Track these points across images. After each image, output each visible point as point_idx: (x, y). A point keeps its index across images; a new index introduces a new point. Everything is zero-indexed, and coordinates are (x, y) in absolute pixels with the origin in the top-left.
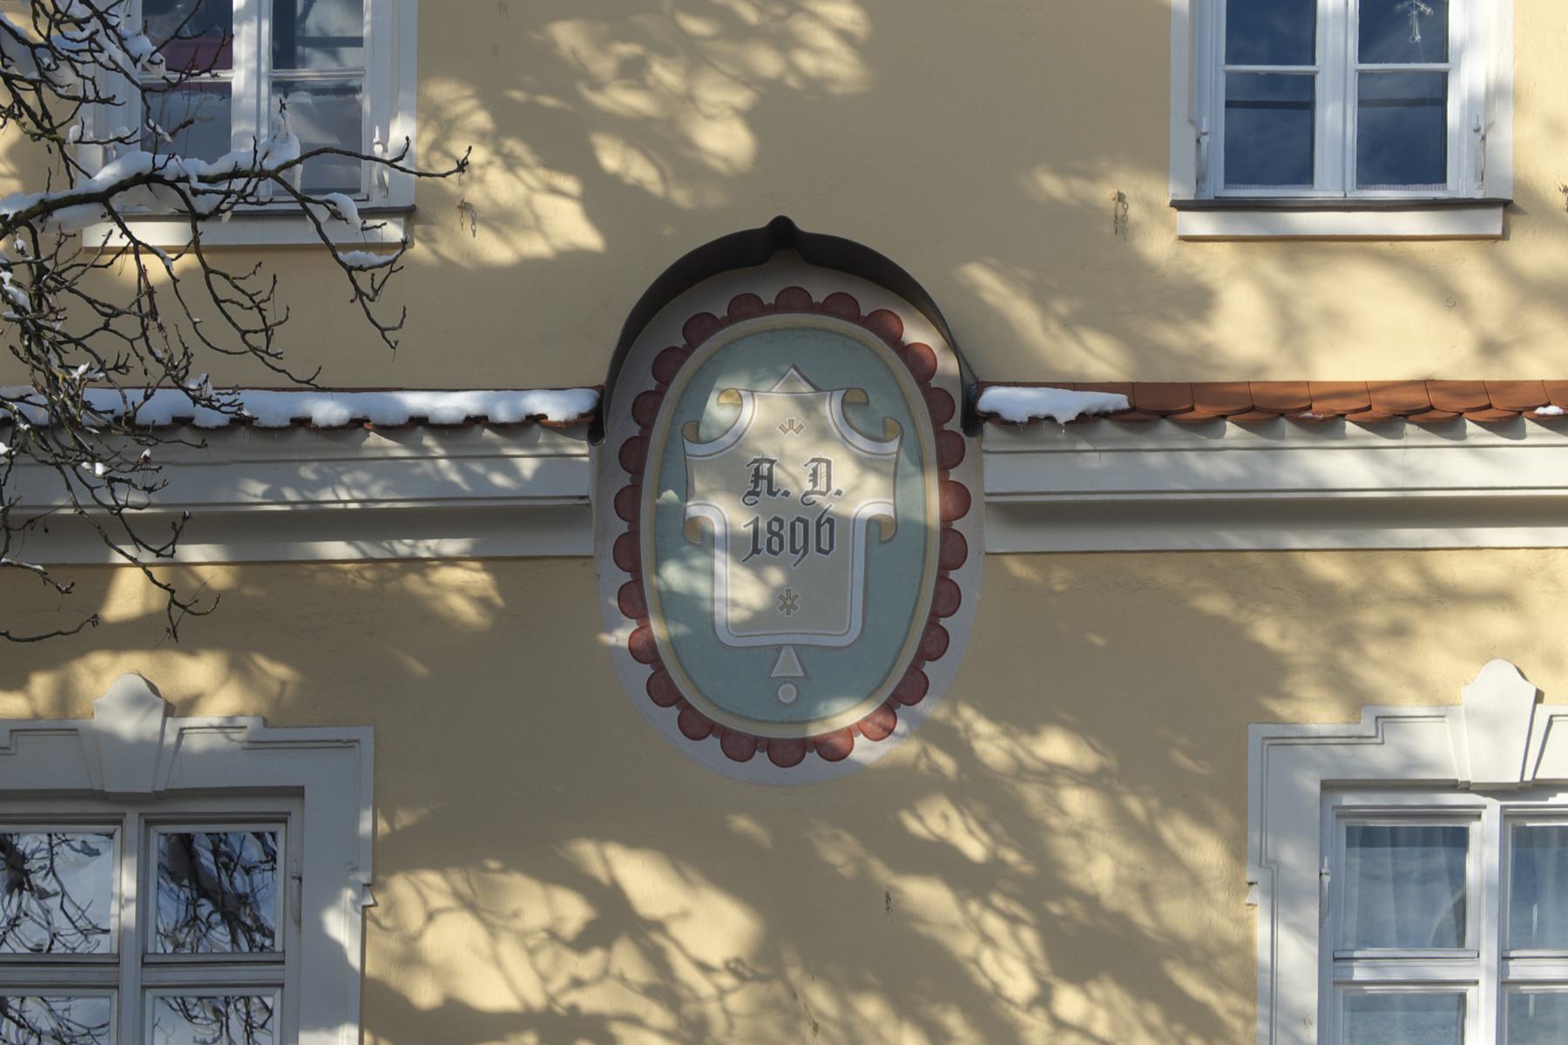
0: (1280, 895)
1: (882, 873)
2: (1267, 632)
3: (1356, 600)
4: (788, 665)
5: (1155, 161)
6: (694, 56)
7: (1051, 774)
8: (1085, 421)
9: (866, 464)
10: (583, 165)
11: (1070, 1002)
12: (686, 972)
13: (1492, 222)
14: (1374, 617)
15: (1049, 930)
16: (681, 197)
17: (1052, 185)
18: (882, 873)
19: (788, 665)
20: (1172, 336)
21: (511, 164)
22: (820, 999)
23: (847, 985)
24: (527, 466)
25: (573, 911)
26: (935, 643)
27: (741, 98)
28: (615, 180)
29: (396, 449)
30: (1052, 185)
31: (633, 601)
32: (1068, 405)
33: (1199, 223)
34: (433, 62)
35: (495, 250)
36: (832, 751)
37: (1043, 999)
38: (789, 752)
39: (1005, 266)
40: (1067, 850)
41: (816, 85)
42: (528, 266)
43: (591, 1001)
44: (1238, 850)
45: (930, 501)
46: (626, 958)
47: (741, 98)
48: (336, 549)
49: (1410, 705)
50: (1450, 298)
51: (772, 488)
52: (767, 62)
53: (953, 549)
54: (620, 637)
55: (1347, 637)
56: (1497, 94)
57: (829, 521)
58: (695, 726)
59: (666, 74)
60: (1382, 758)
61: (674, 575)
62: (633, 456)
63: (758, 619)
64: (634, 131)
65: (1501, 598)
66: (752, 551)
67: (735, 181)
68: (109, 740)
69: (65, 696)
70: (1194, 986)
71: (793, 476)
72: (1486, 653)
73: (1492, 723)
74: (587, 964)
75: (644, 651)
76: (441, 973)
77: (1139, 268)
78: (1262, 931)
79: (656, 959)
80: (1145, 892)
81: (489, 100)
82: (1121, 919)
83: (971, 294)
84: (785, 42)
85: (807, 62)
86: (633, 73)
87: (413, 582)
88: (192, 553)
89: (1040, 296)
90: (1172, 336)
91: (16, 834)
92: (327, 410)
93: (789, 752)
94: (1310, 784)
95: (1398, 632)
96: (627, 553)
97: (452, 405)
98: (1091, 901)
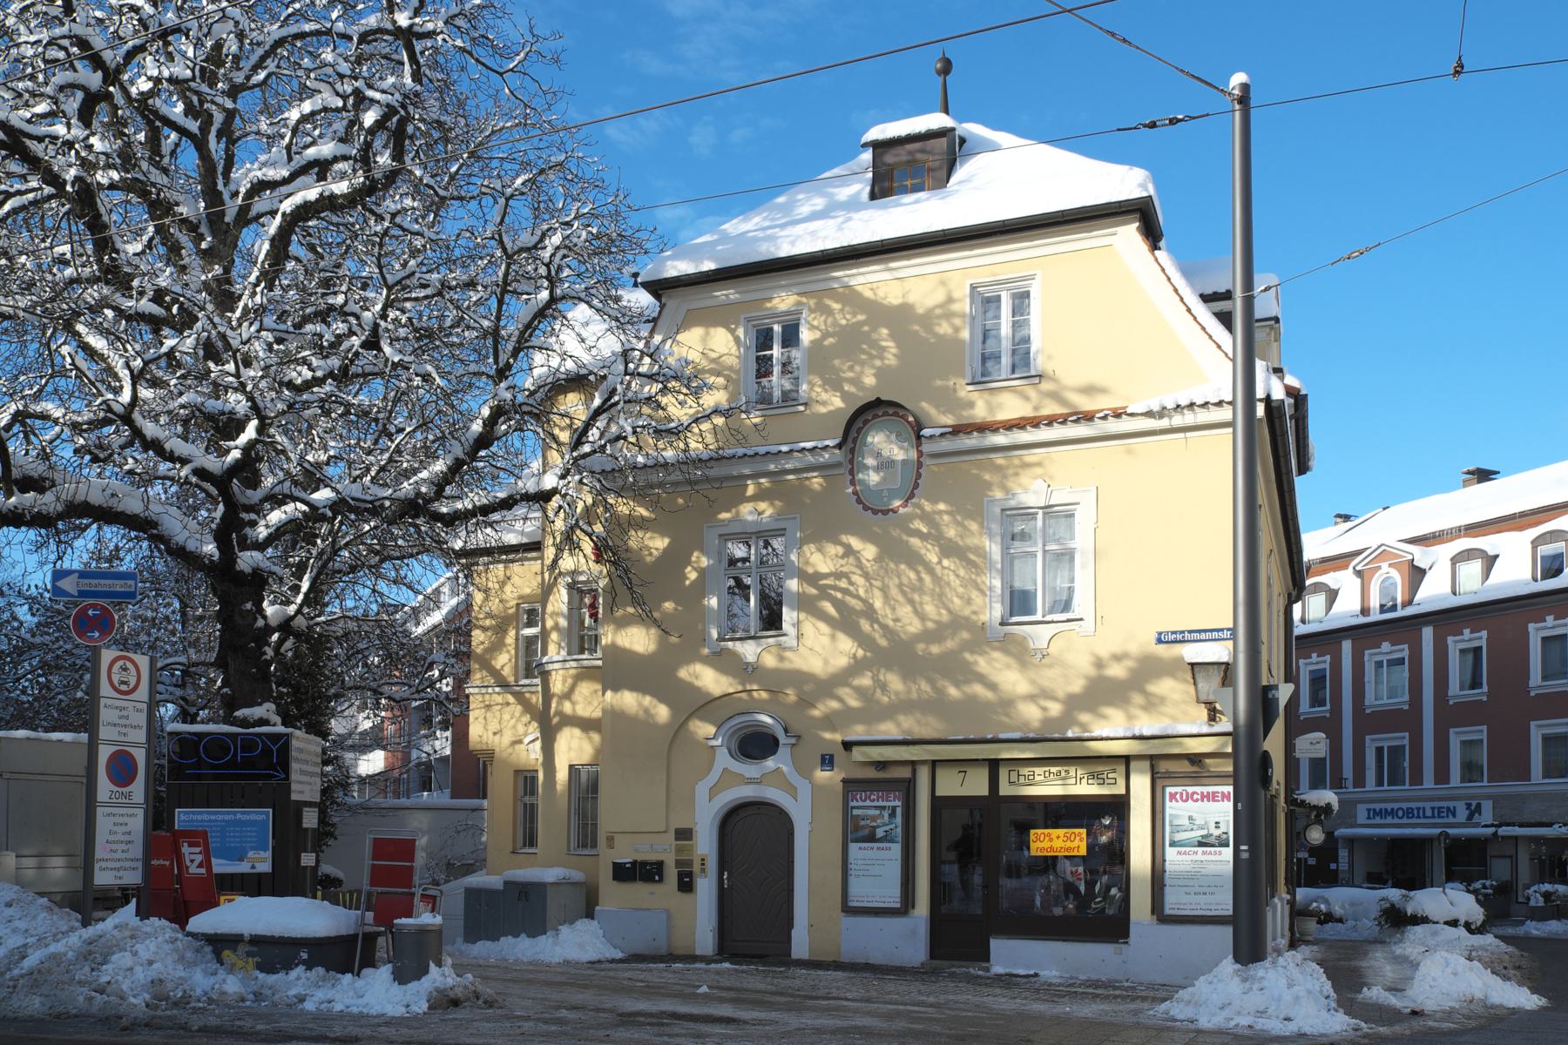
0: (991, 536)
1: (905, 537)
2: (987, 477)
3: (1007, 467)
4: (885, 493)
5: (964, 376)
6: (863, 363)
7: (940, 512)
8: (942, 435)
9: (901, 448)
10: (841, 390)
11: (946, 563)
12: (864, 561)
13: (1036, 380)
14: (1011, 471)
15: (940, 547)
16: (861, 394)
17: (939, 383)
18: (905, 537)
19: (885, 493)
20: (965, 413)
21: (826, 391)
22: (892, 565)
23: (897, 563)
24: (827, 456)
25: (840, 550)
26: (916, 486)
27: (873, 371)
28: (847, 392)
29: (800, 455)
30: (939, 383)
31: (853, 482)
32: (938, 431)
33: (970, 388)
34: (811, 371)
35: (823, 410)
36: (894, 511)
37: (940, 562)
38: (885, 512)
39: (929, 401)
40: (945, 529)
41: (889, 366)
42: (830, 412)
43: (844, 569)
44: (982, 525)
45: (913, 454)
46: (851, 560)
47: (873, 371)
48: (791, 477)
49: (1019, 491)
50: (1027, 398)
51: (260, 876)
52: (878, 363)
53: (920, 465)
54: (850, 490)
55: (1005, 477)
56: (1037, 352)
57: (893, 461)
58: (866, 508)
59: (857, 368)
60: (1012, 503)
61: (860, 476)
62: (852, 451)
63: (878, 484)
64: (852, 381)
65: (1039, 464)
66: (877, 469)
67: (872, 389)
68: (746, 521)
69: (738, 513)
70: (972, 557)
71: (886, 453)
72: (1035, 478)
73: (1036, 493)
74: (843, 562)
75: (855, 493)
76: (813, 566)
77: (960, 399)
78: (988, 543)
79: (858, 559)
80: (961, 537)
81: (822, 378)
82: (956, 543)
83: (922, 409)
84: (882, 358)
85: (886, 362)
86: (851, 368)
87: (807, 483)
88: (762, 480)
89: (937, 407)
90: (965, 413)
91: (111, 900)
92: (785, 448)
93: (885, 512)
94: (998, 510)
95: (1016, 474)
96: (852, 472)
97: (809, 445)
98: (950, 540)
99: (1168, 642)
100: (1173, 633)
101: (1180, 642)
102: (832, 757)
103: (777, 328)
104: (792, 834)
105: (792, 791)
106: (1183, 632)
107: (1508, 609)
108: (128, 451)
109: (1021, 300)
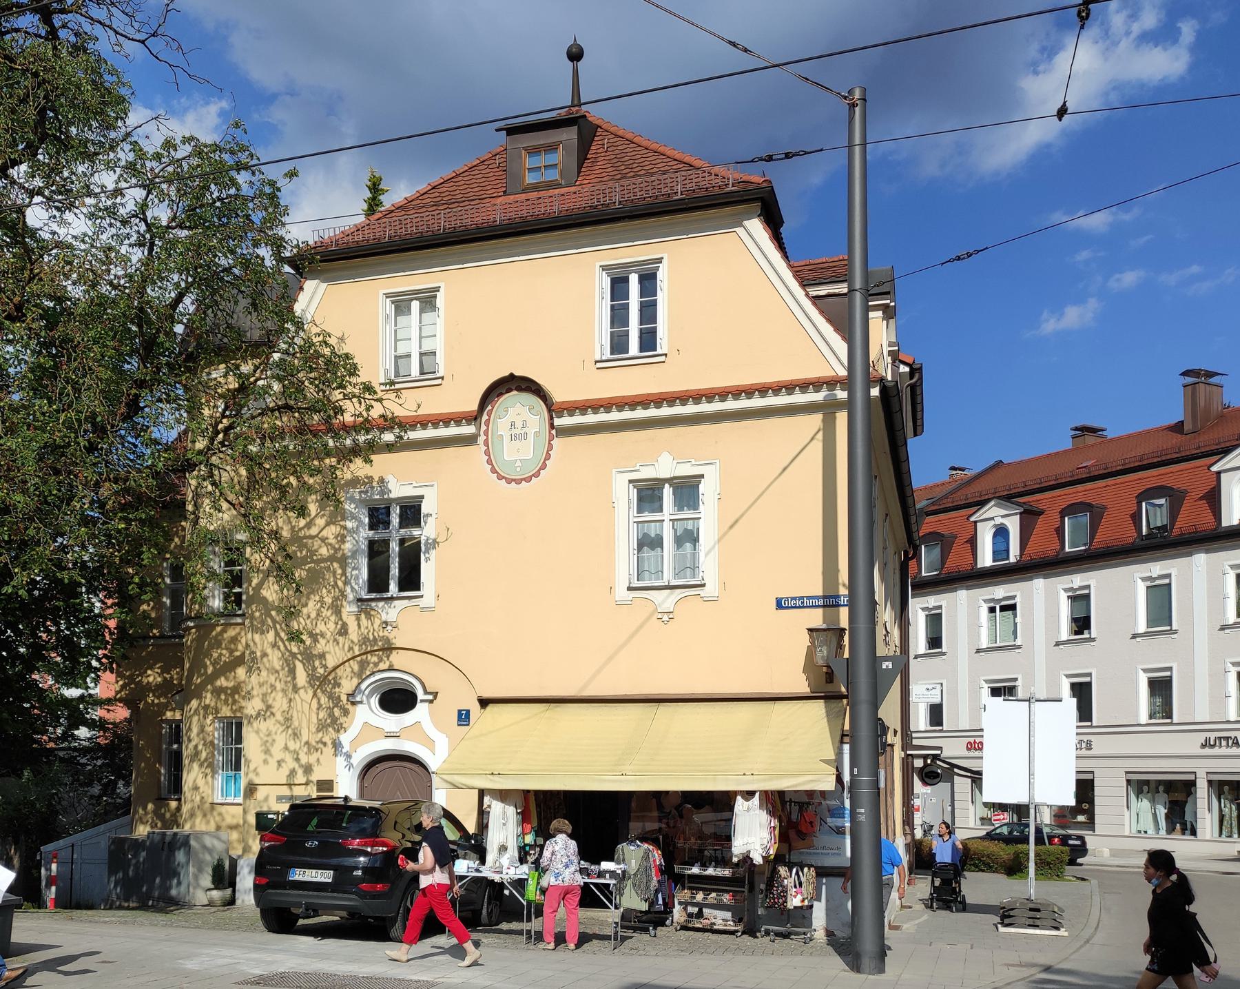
99: (788, 608)
100: (793, 599)
101: (799, 607)
102: (468, 712)
103: (393, 587)
104: (1050, 455)
105: (430, 744)
106: (802, 598)
107: (457, 769)
108: (278, 725)
109: (619, 345)
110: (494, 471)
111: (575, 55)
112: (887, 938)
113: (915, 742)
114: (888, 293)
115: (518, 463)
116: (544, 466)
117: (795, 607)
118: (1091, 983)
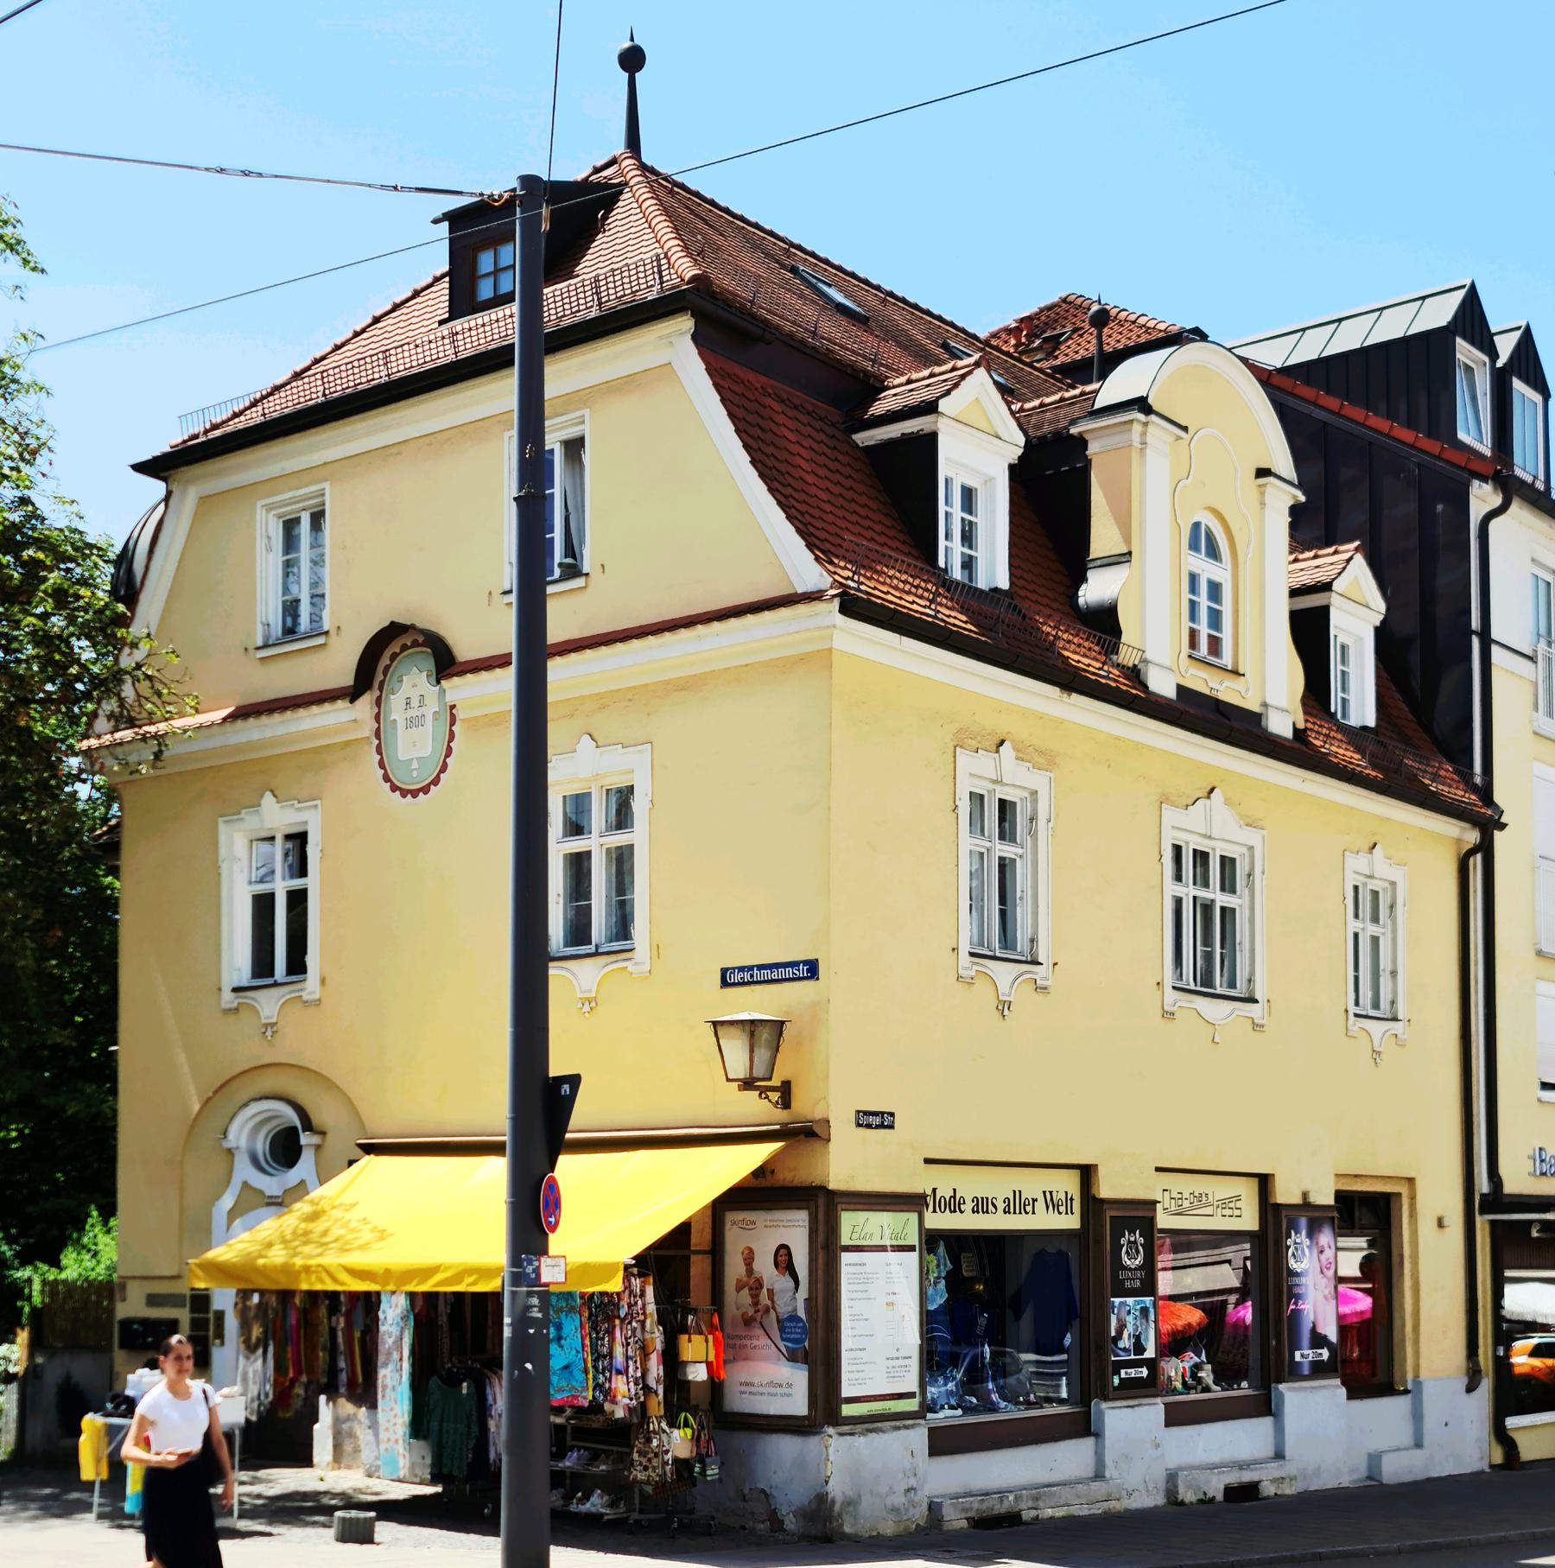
99: (734, 985)
100: (741, 969)
101: (749, 983)
106: (751, 968)
110: (386, 778)
111: (632, 60)
112: (850, 1503)
113: (847, 1410)
114: (1208, 980)
115: (415, 765)
116: (444, 768)
117: (743, 984)
118: (858, 309)
